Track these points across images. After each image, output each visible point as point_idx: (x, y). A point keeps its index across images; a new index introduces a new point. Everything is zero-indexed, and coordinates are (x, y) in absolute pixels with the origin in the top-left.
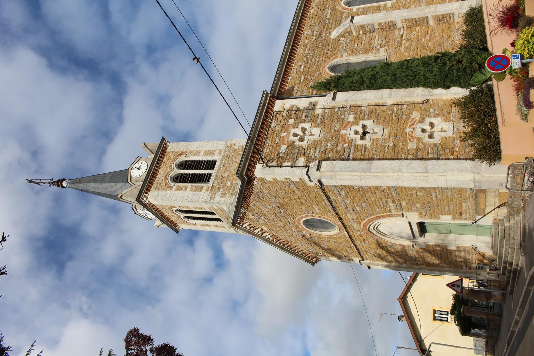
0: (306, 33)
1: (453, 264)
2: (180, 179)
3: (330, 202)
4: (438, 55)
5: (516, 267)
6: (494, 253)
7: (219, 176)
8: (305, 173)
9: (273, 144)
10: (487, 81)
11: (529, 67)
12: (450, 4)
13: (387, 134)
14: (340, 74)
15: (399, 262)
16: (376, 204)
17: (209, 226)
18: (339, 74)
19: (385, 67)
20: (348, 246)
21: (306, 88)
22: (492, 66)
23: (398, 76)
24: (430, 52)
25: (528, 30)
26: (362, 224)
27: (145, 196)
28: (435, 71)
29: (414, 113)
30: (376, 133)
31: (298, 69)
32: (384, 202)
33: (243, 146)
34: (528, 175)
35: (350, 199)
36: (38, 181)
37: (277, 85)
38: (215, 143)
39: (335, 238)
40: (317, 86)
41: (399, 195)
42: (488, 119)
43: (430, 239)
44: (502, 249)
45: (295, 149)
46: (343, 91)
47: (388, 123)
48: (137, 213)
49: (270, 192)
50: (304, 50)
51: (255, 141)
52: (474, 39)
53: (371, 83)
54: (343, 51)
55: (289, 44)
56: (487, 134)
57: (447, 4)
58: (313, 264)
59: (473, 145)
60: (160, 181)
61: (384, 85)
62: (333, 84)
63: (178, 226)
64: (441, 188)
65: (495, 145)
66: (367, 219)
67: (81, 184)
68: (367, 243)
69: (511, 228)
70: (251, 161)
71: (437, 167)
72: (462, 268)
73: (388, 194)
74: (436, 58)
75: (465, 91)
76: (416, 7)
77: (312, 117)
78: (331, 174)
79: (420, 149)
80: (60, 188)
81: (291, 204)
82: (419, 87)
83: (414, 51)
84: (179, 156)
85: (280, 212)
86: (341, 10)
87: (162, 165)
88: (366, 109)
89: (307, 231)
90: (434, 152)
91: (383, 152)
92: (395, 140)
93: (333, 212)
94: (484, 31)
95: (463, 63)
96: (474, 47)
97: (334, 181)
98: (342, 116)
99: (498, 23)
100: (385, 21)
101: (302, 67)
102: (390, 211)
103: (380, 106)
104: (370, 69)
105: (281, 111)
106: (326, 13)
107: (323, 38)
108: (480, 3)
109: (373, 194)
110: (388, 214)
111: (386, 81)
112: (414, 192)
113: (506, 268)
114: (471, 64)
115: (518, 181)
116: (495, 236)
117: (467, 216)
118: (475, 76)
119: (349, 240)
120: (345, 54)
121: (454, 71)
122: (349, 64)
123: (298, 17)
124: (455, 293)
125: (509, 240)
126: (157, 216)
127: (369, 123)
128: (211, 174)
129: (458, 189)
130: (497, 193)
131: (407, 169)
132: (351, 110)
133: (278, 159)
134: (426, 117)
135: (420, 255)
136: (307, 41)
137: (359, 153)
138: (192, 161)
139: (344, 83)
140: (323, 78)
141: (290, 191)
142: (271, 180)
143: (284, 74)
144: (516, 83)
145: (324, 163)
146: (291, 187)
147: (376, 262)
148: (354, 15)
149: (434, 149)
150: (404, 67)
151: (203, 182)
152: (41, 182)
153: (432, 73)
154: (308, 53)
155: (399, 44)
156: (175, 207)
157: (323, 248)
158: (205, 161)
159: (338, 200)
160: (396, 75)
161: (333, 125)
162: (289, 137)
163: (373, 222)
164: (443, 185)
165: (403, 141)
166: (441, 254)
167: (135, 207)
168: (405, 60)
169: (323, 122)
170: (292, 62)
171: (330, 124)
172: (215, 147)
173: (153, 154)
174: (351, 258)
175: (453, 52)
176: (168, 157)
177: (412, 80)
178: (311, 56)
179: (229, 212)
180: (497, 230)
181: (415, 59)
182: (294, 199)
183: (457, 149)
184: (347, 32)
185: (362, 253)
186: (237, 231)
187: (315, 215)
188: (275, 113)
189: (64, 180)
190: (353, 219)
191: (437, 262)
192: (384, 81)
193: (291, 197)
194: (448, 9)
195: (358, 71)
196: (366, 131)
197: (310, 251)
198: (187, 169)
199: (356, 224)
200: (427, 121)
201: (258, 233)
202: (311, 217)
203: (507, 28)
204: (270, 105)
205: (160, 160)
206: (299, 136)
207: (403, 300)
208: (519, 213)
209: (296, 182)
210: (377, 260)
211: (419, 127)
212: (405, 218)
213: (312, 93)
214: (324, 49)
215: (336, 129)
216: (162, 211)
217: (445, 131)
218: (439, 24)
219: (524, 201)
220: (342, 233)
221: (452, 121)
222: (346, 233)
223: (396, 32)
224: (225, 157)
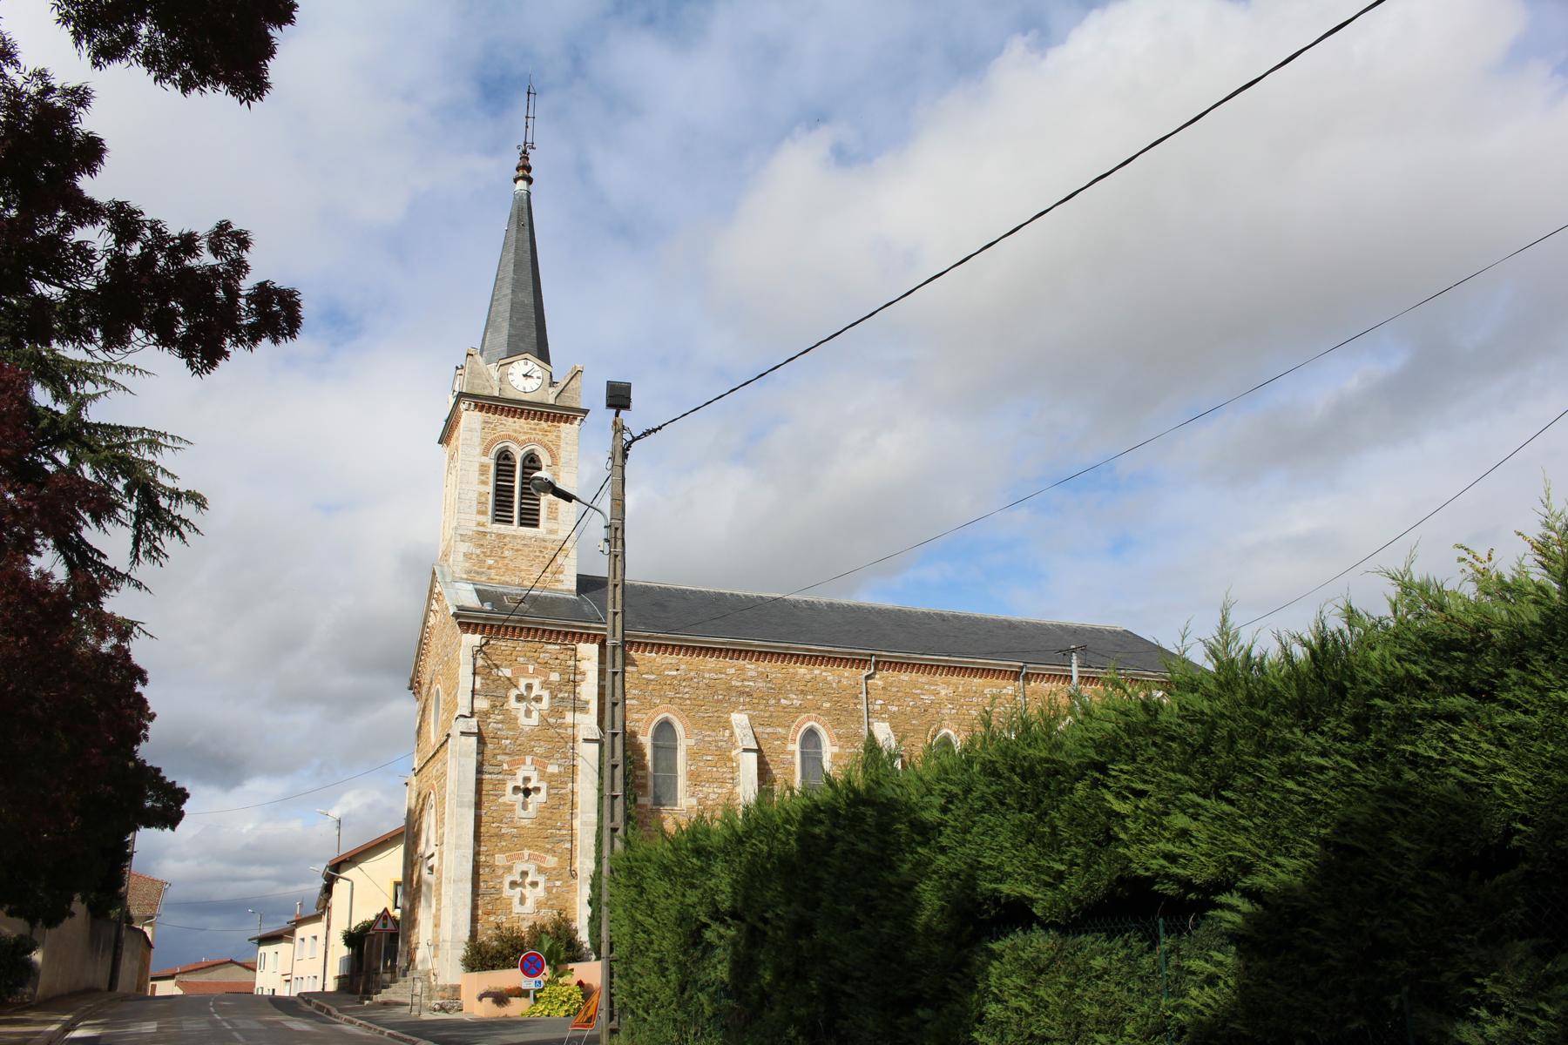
0: (753, 666)
2: (504, 458)
9: (515, 653)
29: (556, 859)
31: (670, 666)
50: (710, 671)
70: (484, 626)
101: (675, 673)
127: (542, 796)
136: (733, 671)
161: (542, 743)
183: (492, 919)
189: (530, 181)
224: (543, 544)
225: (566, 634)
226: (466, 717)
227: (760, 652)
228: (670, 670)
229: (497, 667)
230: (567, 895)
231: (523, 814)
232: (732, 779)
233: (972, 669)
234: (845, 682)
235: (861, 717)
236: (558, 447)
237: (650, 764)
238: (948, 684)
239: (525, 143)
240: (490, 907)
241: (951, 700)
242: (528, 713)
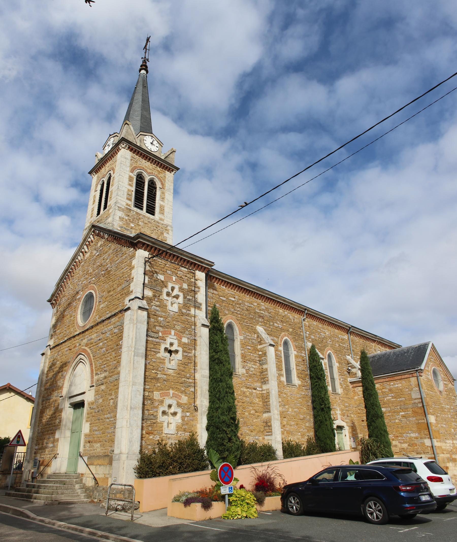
1: (41, 436)
2: (140, 180)
3: (109, 318)
4: (237, 421)
5: (33, 497)
6: (49, 475)
7: (140, 217)
8: (137, 296)
9: (166, 268)
10: (212, 464)
11: (221, 501)
12: (280, 432)
13: (169, 373)
14: (225, 332)
15: (47, 383)
16: (104, 361)
17: (94, 204)
18: (225, 331)
19: (229, 372)
20: (65, 334)
21: (214, 301)
22: (224, 468)
23: (220, 384)
24: (240, 414)
25: (253, 499)
26: (86, 348)
27: (126, 146)
28: (223, 417)
29: (187, 398)
30: (170, 363)
31: (231, 295)
32: (106, 369)
33: (166, 241)
34: (123, 504)
35: (110, 336)
36: (148, 47)
37: (219, 275)
39: (74, 322)
40: (215, 311)
41: (111, 383)
42: (177, 466)
43: (68, 413)
44: (53, 483)
45: (160, 288)
46: (210, 334)
47: (179, 374)
49: (122, 262)
50: (248, 302)
51: (170, 252)
52: (249, 453)
53: (215, 360)
54: (245, 336)
55: (254, 289)
56: (164, 465)
57: (281, 430)
58: (49, 301)
59: (154, 452)
60: (139, 162)
61: (212, 371)
62: (216, 325)
63: (95, 174)
64: (116, 423)
65: (153, 473)
66: (90, 353)
67: (141, 88)
68: (67, 353)
69: (73, 491)
72: (36, 445)
73: (112, 372)
74: (234, 419)
75: (203, 444)
76: (280, 402)
77: (188, 305)
78: (135, 319)
79: (153, 403)
80: (140, 67)
81: (108, 281)
82: (209, 402)
83: (241, 399)
84: (161, 182)
85: (102, 270)
88: (192, 354)
89: (82, 296)
90: (150, 416)
91: (152, 368)
92: (163, 380)
93: (99, 320)
94: (255, 462)
95: (229, 443)
96: (242, 453)
97: (128, 322)
98: (187, 332)
99: (261, 474)
100: (269, 375)
101: (233, 299)
102: (97, 374)
103: (195, 367)
104: (227, 359)
105: (195, 277)
106: (279, 323)
107: (257, 319)
108: (279, 459)
109: (114, 358)
110: (94, 372)
111: (216, 373)
112: (113, 397)
113: (34, 488)
114: (227, 450)
115: (118, 496)
116: (66, 476)
117: (87, 448)
118: (216, 453)
119: (72, 336)
120: (242, 338)
121: (222, 435)
122: (233, 340)
123: (277, 298)
124: (11, 439)
125: (61, 489)
126: (106, 155)
127: (179, 356)
128: (142, 209)
129: (114, 439)
130: (108, 476)
131: (135, 390)
132: (192, 340)
133: (152, 272)
134: (182, 409)
135: (52, 404)
137: (152, 346)
138: (155, 193)
139: (216, 335)
140: (222, 317)
141: (121, 281)
142: (133, 264)
143: (228, 283)
144: (208, 490)
145: (145, 313)
146: (125, 282)
147: (48, 361)
148: (276, 347)
149: (152, 416)
150: (227, 390)
151: (135, 201)
152: (146, 50)
153: (221, 415)
154: (245, 305)
155: (248, 386)
156: (114, 173)
157: (64, 311)
158: (155, 205)
159: (110, 325)
160: (221, 382)
161: (179, 323)
162: (171, 283)
163: (87, 358)
164: (118, 425)
165: (161, 387)
166: (52, 424)
167: (116, 136)
168: (234, 391)
169: (183, 314)
170: (238, 290)
172: (167, 215)
173: (165, 158)
174: (53, 337)
175: (239, 435)
177: (216, 396)
178: (242, 308)
179: (105, 224)
180: (72, 478)
181: (234, 399)
182: (113, 284)
183: (151, 437)
185: (58, 348)
186: (86, 229)
187: (97, 304)
189: (147, 72)
191: (44, 420)
192: (216, 371)
193: (116, 282)
194: (276, 430)
195: (227, 348)
196: (173, 353)
197: (63, 298)
198: (148, 188)
200: (178, 409)
201: (83, 248)
202: (96, 300)
203: (256, 482)
204: (201, 268)
205: (158, 164)
206: (171, 292)
207: (8, 388)
208: (88, 498)
209: (130, 287)
210: (49, 362)
211: (173, 402)
212: (90, 389)
213: (209, 306)
214: (248, 319)
215: (176, 326)
216: (111, 161)
217: (168, 427)
218: (264, 422)
219: (99, 502)
220: (79, 329)
221: (177, 432)
222: (78, 333)
223: (259, 384)
224: (157, 224)
228: (232, 297)
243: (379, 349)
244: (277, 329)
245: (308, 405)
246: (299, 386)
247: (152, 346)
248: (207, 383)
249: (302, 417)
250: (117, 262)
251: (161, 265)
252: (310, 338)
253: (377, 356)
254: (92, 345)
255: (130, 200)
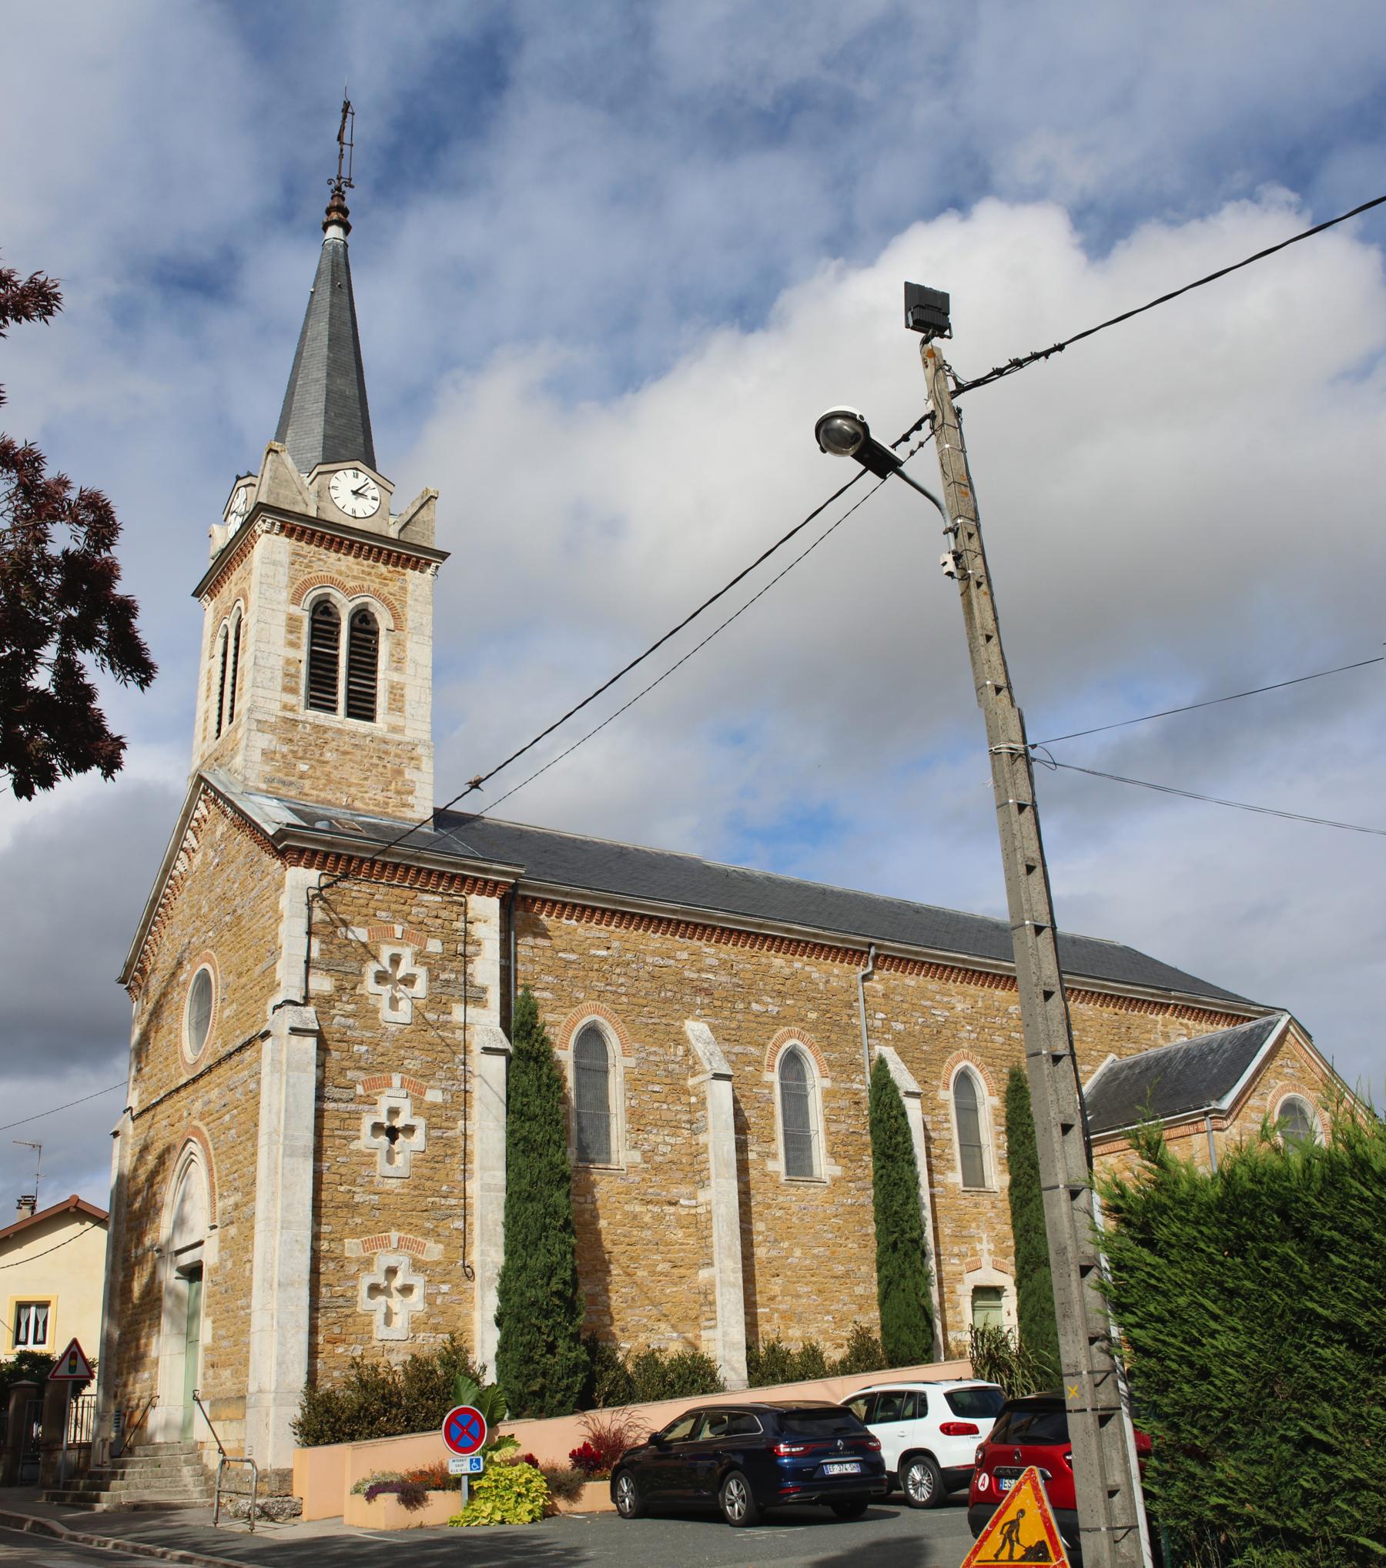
0: (712, 950)
2: (323, 615)
3: (240, 1049)
7: (326, 736)
9: (373, 904)
13: (388, 1187)
22: (459, 1418)
23: (529, 1205)
27: (273, 524)
29: (441, 1246)
32: (236, 1184)
36: (346, 139)
38: (425, 711)
45: (355, 965)
48: (241, 483)
50: (654, 953)
54: (643, 1055)
60: (316, 565)
69: (175, 1481)
70: (326, 855)
71: (292, 1308)
78: (284, 1061)
83: (625, 1236)
86: (774, 1040)
87: (365, 562)
93: (223, 1052)
95: (548, 1356)
101: (604, 953)
102: (221, 1196)
103: (465, 1164)
106: (770, 1000)
118: (470, 1384)
127: (418, 1140)
128: (334, 710)
136: (685, 955)
137: (337, 1123)
143: (584, 908)
149: (341, 1299)
155: (649, 1197)
161: (417, 1053)
162: (389, 943)
171: (421, 1046)
176: (390, 575)
183: (340, 1350)
184: (695, 1063)
188: (463, 900)
189: (347, 228)
190: (210, 1102)
198: (352, 637)
199: (200, 1108)
207: (73, 1210)
211: (401, 1261)
214: (654, 1004)
215: (406, 1062)
224: (383, 746)
225: (453, 877)
226: (296, 1004)
227: (723, 929)
228: (598, 947)
229: (345, 924)
230: (458, 1309)
231: (389, 1170)
232: (690, 1122)
233: (995, 975)
234: (834, 982)
235: (857, 1036)
236: (403, 603)
237: (572, 1095)
238: (964, 995)
239: (339, 178)
240: (336, 1330)
241: (970, 1020)
242: (394, 1002)
243: (1185, 1032)
244: (760, 1019)
245: (868, 1235)
246: (835, 1181)
247: (337, 1123)
248: (499, 1204)
249: (840, 1269)
250: (253, 894)
251: (358, 898)
252: (889, 1030)
253: (1227, 1046)
254: (211, 1118)
255: (293, 691)
